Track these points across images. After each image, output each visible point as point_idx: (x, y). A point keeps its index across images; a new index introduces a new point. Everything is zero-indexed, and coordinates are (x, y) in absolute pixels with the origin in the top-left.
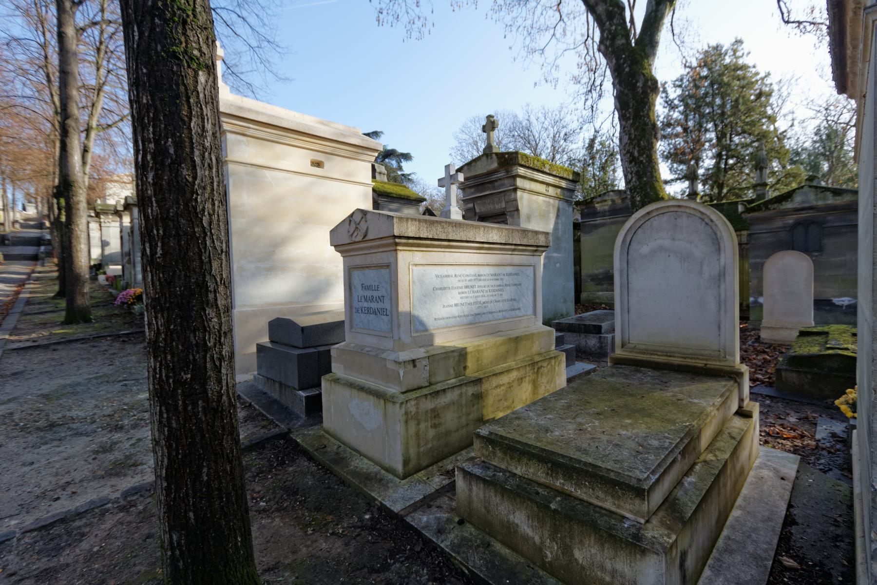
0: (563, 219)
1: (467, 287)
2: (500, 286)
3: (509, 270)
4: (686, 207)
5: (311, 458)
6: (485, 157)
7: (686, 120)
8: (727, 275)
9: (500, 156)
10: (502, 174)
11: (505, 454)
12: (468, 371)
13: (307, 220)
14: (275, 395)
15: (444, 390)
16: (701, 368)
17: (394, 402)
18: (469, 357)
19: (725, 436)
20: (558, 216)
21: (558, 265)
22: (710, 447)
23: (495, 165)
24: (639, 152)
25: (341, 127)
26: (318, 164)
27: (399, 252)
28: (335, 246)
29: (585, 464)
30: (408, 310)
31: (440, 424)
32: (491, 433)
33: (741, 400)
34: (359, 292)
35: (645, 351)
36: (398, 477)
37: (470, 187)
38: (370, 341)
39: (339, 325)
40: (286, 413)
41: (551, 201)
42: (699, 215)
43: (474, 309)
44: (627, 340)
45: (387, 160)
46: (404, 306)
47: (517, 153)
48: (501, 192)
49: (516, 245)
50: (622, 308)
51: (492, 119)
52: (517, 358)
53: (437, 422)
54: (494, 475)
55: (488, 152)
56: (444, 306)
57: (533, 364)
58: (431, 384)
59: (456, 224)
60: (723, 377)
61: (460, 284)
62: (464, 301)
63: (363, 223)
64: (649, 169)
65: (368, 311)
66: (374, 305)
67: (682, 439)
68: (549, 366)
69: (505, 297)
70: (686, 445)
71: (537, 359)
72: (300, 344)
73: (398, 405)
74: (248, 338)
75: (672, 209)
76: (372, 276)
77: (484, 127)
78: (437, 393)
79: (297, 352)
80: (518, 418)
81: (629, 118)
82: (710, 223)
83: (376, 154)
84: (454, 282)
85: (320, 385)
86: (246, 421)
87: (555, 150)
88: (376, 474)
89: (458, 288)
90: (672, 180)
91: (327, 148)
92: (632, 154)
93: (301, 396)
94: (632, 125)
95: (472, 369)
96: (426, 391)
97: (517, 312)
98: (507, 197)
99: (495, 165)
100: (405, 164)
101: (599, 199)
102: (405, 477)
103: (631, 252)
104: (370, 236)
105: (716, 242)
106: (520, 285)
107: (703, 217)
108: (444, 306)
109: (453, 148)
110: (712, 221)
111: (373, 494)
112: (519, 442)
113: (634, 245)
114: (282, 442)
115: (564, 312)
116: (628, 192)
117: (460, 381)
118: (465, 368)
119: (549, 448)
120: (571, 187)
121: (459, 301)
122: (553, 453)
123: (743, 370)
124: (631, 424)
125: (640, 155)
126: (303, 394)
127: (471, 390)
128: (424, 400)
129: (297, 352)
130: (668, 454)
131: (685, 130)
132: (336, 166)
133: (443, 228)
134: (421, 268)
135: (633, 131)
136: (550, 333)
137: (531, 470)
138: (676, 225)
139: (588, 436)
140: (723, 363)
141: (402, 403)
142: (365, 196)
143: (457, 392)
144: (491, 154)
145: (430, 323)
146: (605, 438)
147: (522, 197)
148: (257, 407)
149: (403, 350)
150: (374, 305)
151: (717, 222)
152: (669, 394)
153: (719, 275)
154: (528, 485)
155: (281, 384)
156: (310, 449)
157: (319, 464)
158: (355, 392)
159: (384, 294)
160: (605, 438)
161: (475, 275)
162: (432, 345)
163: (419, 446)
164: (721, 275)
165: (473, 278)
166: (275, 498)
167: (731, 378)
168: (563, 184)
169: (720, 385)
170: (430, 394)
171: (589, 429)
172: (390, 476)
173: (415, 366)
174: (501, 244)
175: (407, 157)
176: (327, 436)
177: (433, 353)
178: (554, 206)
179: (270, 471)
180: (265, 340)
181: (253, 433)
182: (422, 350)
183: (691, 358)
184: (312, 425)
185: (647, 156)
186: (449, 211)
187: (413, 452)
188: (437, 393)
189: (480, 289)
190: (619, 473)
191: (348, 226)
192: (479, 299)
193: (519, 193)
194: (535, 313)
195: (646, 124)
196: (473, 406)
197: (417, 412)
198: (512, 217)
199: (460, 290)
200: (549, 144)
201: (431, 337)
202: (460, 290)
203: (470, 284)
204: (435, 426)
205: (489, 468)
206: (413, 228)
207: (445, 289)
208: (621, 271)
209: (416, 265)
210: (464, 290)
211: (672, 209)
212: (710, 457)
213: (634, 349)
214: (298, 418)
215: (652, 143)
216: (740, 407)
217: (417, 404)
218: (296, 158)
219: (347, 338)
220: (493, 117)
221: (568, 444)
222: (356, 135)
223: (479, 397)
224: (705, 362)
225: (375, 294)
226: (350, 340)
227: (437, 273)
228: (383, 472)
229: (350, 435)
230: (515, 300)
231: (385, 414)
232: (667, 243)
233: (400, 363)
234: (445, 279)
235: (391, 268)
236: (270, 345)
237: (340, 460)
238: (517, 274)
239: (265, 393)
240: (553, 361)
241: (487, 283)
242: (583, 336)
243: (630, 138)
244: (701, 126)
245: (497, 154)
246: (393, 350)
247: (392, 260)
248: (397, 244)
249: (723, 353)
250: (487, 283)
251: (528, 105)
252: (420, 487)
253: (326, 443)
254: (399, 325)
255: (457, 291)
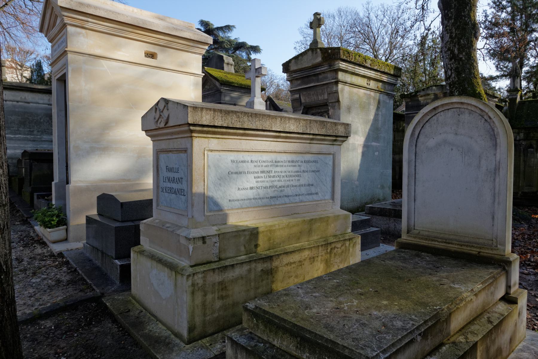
0: (384, 111)
1: (262, 172)
2: (297, 172)
3: (308, 157)
4: (468, 104)
5: (115, 321)
6: (310, 52)
7: (513, 19)
8: (501, 169)
9: (324, 51)
10: (325, 68)
11: (266, 327)
12: (259, 249)
13: (131, 104)
14: (98, 263)
15: (233, 266)
16: (475, 256)
17: (182, 274)
18: (261, 237)
19: (484, 320)
20: (378, 108)
21: (377, 153)
22: (462, 330)
23: (319, 59)
24: (459, 50)
25: (176, 22)
26: (151, 55)
27: (194, 138)
28: (146, 131)
29: (327, 340)
30: (202, 191)
31: (227, 296)
32: (256, 307)
33: (508, 287)
34: (164, 173)
35: (427, 238)
36: (184, 342)
37: (297, 79)
38: (171, 218)
39: (149, 202)
40: (103, 277)
41: (372, 94)
42: (479, 111)
43: (271, 193)
44: (412, 227)
45: (238, 52)
46: (198, 188)
47: (339, 49)
48: (324, 84)
49: (313, 134)
50: (408, 196)
51: (318, 17)
52: (311, 239)
53: (224, 294)
54: (256, 345)
55: (314, 47)
56: (239, 189)
57: (327, 244)
58: (220, 259)
59: (257, 115)
60: (494, 264)
61: (257, 169)
62: (259, 185)
63: (165, 110)
64: (468, 66)
65: (171, 191)
66: (175, 186)
67: (426, 322)
68: (343, 248)
69: (302, 182)
70: (430, 327)
71: (331, 240)
72: (120, 218)
73: (185, 277)
74: (81, 211)
75: (456, 106)
76: (173, 159)
77: (311, 23)
78: (225, 268)
79: (118, 224)
80: (286, 295)
81: (450, 18)
82: (489, 120)
83: (207, 47)
84: (251, 167)
85: (130, 257)
86: (68, 285)
87: (392, 46)
88: (166, 338)
89: (254, 173)
90: (498, 76)
91: (162, 41)
92: (452, 52)
93: (116, 264)
94: (453, 24)
95: (263, 248)
96: (214, 266)
97: (315, 197)
98: (329, 90)
99: (319, 59)
100: (253, 56)
101: (422, 93)
102: (189, 342)
103: (419, 144)
104: (171, 124)
105: (494, 137)
106: (318, 171)
107: (483, 114)
108: (239, 189)
109: (297, 42)
110: (490, 118)
111: (158, 356)
112: (277, 317)
113: (422, 138)
114: (94, 304)
115: (381, 197)
116: (448, 88)
117: (250, 258)
118: (256, 246)
119: (301, 324)
120: (392, 80)
121: (255, 185)
122: (302, 329)
123: (511, 259)
124: (386, 306)
125: (460, 52)
126: (118, 262)
127: (260, 267)
128: (212, 273)
129: (118, 224)
130: (407, 335)
131: (513, 30)
132: (165, 58)
133: (238, 117)
134: (217, 153)
135: (454, 31)
136: (346, 217)
137: (285, 343)
138: (459, 121)
139: (342, 314)
140: (495, 252)
141: (189, 276)
142: (196, 84)
143: (246, 268)
144: (317, 49)
145: (224, 204)
146: (355, 317)
147: (343, 90)
148: (80, 272)
149: (196, 228)
150: (175, 186)
151: (494, 119)
152: (435, 279)
153: (495, 170)
154: (282, 356)
155: (103, 253)
156: (115, 313)
157: (121, 327)
158: (155, 263)
159: (183, 176)
160: (355, 317)
161: (272, 162)
162: (226, 224)
163: (205, 315)
164: (497, 169)
165: (270, 164)
166: (75, 354)
167: (500, 266)
168: (385, 78)
169: (486, 273)
170: (218, 268)
171: (346, 308)
172: (178, 341)
173: (204, 242)
174: (298, 133)
175: (256, 49)
176: (134, 301)
177: (223, 231)
178: (374, 99)
179: (78, 330)
180: (94, 212)
181: (71, 296)
182: (215, 228)
183: (467, 246)
184: (124, 291)
185: (466, 54)
186: (253, 101)
187: (198, 320)
188: (225, 268)
189: (277, 174)
190: (353, 350)
191: (154, 113)
192: (275, 184)
193: (340, 86)
194: (333, 198)
195: (467, 24)
196: (262, 281)
197: (205, 284)
198: (333, 107)
199: (256, 175)
200: (387, 40)
201: (225, 217)
202: (256, 175)
203: (266, 169)
204: (222, 298)
205: (253, 339)
206: (208, 117)
207: (241, 173)
208: (409, 163)
209: (212, 151)
210: (260, 175)
211: (456, 106)
212: (461, 339)
213: (418, 235)
214: (113, 283)
215: (472, 42)
216: (507, 293)
217: (204, 277)
218: (133, 50)
219: (154, 215)
220: (319, 14)
221: (319, 321)
222: (189, 28)
223: (270, 273)
224: (478, 250)
225: (176, 176)
226: (158, 215)
227: (232, 158)
228: (173, 336)
229: (151, 302)
230: (312, 185)
231: (176, 285)
232: (451, 137)
233: (190, 239)
234: (241, 164)
235: (187, 151)
236: (97, 218)
237: (139, 323)
238: (315, 162)
239: (90, 260)
240: (347, 243)
241: (284, 169)
242: (392, 220)
243: (451, 37)
244: (527, 26)
245: (321, 49)
246: (187, 228)
247: (188, 146)
248: (192, 131)
249: (496, 242)
250: (284, 169)
251: (368, 3)
252: (201, 352)
253: (130, 308)
254: (193, 205)
255: (252, 176)
